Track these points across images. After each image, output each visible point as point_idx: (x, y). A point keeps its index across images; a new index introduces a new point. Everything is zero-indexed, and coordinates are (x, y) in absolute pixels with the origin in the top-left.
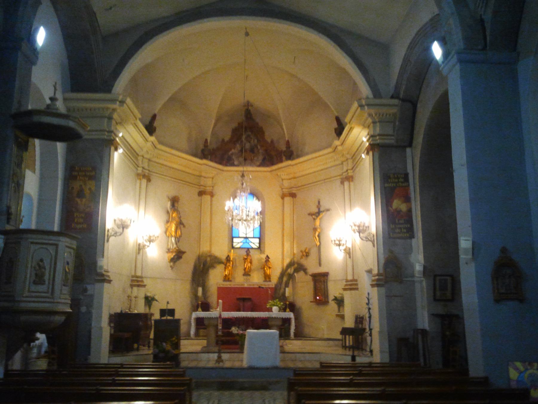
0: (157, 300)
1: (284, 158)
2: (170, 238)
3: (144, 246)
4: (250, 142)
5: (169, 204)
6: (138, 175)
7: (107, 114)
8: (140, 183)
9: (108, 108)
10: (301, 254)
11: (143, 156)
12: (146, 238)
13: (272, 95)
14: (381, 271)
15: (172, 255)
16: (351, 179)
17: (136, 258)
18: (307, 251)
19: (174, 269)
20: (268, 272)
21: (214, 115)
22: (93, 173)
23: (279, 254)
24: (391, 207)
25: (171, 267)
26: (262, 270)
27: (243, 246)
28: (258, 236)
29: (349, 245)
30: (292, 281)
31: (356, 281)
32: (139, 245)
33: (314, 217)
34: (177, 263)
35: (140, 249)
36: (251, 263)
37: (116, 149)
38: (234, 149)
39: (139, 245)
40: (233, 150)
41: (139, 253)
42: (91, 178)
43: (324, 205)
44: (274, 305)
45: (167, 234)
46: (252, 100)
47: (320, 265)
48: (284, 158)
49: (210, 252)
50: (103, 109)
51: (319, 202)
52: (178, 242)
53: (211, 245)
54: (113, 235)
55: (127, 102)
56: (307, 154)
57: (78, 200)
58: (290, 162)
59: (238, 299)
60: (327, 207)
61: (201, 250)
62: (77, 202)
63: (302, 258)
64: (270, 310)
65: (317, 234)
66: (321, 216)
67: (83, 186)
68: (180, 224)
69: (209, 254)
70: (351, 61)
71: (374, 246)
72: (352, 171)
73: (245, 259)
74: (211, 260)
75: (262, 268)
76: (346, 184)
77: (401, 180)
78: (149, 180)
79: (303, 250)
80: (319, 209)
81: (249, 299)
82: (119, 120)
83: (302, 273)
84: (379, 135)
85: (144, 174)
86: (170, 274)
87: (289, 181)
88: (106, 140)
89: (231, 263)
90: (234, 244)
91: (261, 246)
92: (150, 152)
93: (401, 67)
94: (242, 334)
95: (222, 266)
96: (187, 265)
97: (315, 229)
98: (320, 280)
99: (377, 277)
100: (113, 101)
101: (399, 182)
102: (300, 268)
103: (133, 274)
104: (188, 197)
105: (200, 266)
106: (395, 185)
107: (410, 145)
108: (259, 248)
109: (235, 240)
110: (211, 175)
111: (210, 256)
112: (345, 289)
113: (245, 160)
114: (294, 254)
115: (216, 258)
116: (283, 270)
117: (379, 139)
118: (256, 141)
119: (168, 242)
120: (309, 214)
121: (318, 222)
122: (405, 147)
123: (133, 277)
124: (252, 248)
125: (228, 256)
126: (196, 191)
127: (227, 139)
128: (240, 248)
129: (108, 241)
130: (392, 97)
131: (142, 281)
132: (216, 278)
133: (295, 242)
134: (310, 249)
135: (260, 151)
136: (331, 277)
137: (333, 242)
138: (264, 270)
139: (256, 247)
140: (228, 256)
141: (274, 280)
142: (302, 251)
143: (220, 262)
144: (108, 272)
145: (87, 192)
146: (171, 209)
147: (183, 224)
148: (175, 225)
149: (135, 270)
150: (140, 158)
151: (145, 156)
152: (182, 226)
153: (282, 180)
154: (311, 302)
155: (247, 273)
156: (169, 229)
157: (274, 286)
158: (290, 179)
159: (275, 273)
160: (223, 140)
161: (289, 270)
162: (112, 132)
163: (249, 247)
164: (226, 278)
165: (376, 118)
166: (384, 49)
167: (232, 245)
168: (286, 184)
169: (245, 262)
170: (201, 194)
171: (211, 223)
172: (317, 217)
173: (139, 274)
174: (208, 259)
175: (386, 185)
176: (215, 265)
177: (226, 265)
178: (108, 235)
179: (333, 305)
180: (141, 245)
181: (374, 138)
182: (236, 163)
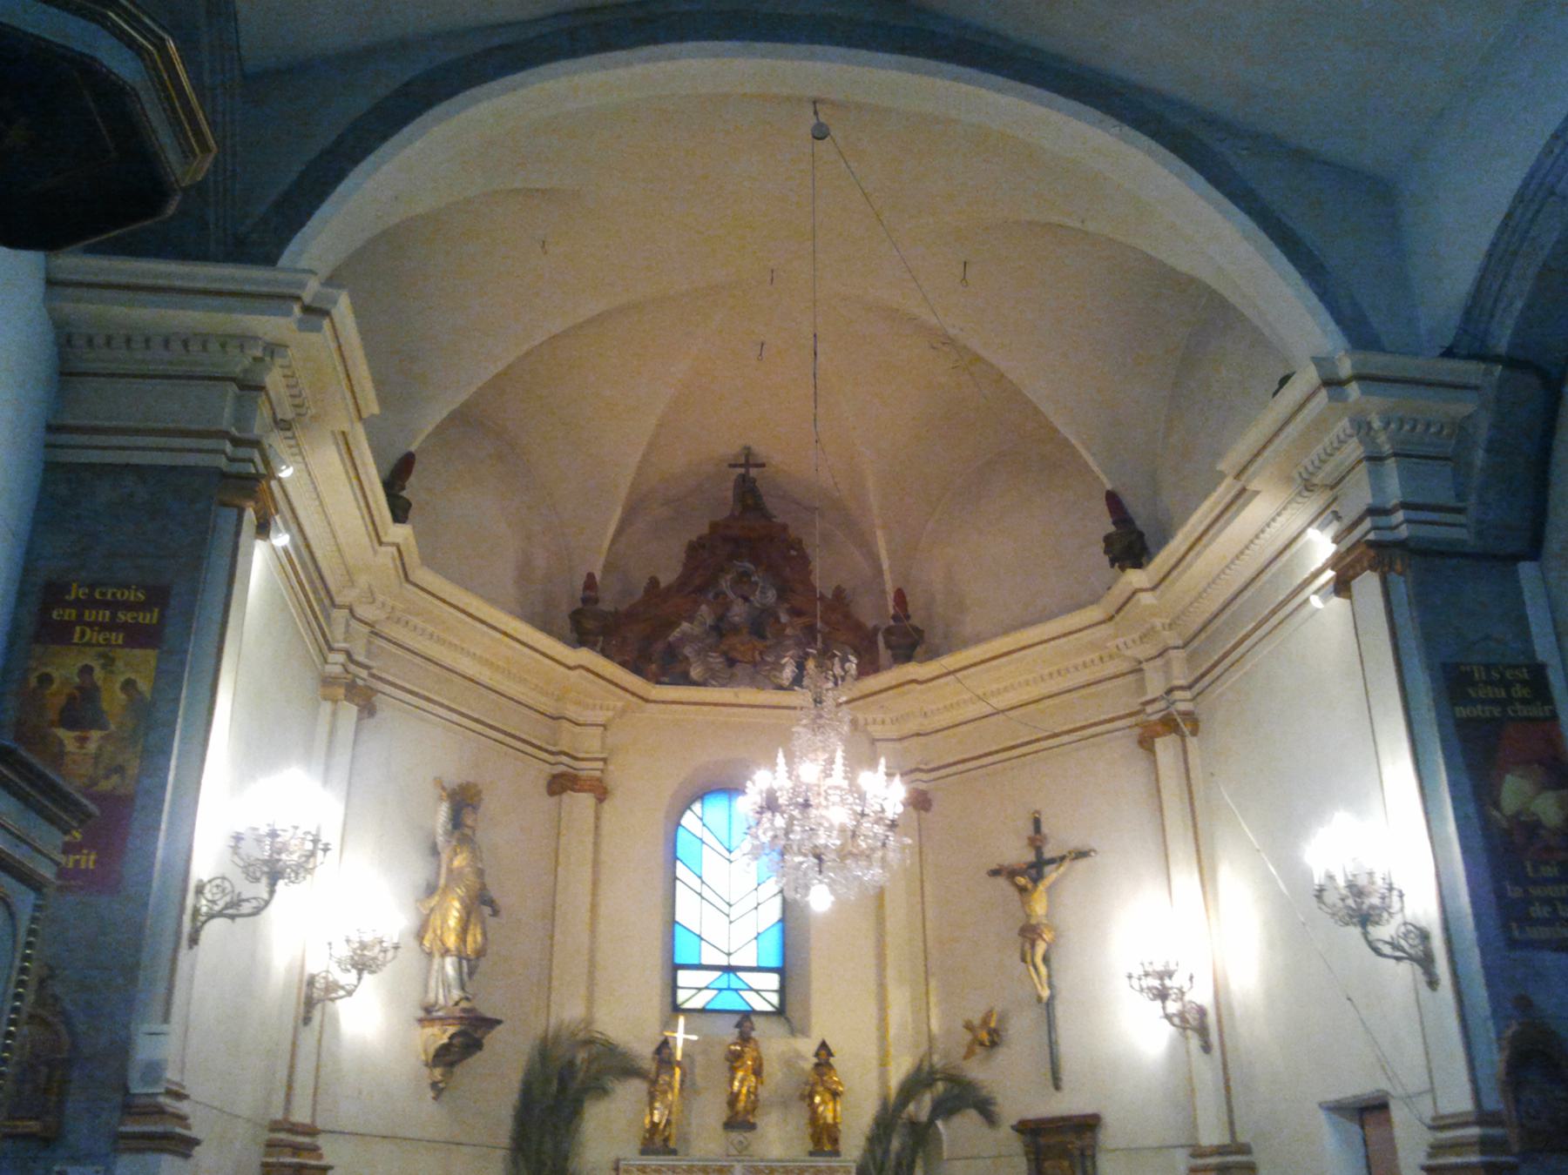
1: (884, 653)
2: (437, 960)
3: (332, 988)
4: (746, 599)
5: (443, 812)
6: (327, 682)
7: (239, 363)
8: (334, 714)
9: (244, 340)
10: (968, 1036)
11: (351, 611)
12: (344, 952)
13: (841, 430)
14: (1494, 1101)
15: (440, 1035)
17: (294, 1044)
18: (993, 1025)
19: (446, 1096)
20: (827, 1112)
21: (623, 493)
22: (149, 618)
24: (1497, 805)
25: (434, 1085)
26: (805, 1105)
28: (774, 960)
29: (1201, 995)
31: (1244, 1149)
32: (311, 982)
33: (1021, 880)
34: (458, 1069)
35: (313, 1000)
36: (757, 1072)
37: (263, 529)
38: (691, 619)
39: (311, 982)
40: (685, 625)
41: (307, 1020)
42: (140, 637)
45: (427, 943)
46: (761, 450)
47: (1057, 1083)
48: (884, 653)
49: (589, 1022)
50: (224, 341)
51: (1037, 823)
52: (471, 974)
53: (590, 1001)
54: (220, 914)
55: (334, 312)
56: (978, 640)
57: (67, 736)
58: (912, 670)
60: (1075, 841)
61: (553, 1021)
62: (61, 743)
63: (969, 1053)
65: (1041, 948)
66: (1052, 874)
67: (98, 674)
68: (481, 903)
69: (582, 1036)
70: (1251, 225)
71: (1433, 983)
72: (1188, 694)
77: (1519, 691)
79: (977, 1021)
80: (1039, 851)
82: (287, 412)
84: (1404, 506)
85: (349, 680)
86: (427, 1115)
88: (224, 475)
89: (678, 1071)
90: (682, 996)
91: (790, 998)
92: (380, 598)
93: (1505, 224)
95: (637, 1087)
99: (1474, 1131)
100: (278, 300)
101: (1510, 700)
102: (961, 1096)
103: (279, 1116)
104: (513, 792)
106: (1497, 712)
107: (1534, 549)
108: (780, 1012)
109: (684, 977)
110: (601, 716)
111: (589, 1042)
113: (731, 662)
114: (931, 1039)
115: (610, 1049)
117: (1408, 521)
118: (771, 595)
120: (995, 873)
121: (1039, 906)
122: (1516, 558)
123: (275, 1126)
124: (754, 1012)
126: (538, 772)
127: (666, 578)
128: (703, 1011)
129: (194, 940)
130: (1449, 353)
131: (314, 1150)
133: (933, 983)
134: (1003, 1018)
135: (788, 631)
136: (1109, 1137)
138: (813, 1107)
139: (770, 1008)
142: (969, 1026)
143: (627, 1068)
144: (180, 1096)
145: (113, 700)
146: (449, 834)
147: (490, 903)
150: (340, 615)
151: (360, 611)
152: (487, 910)
155: (739, 1121)
156: (436, 921)
158: (901, 739)
160: (654, 582)
161: (911, 1107)
162: (256, 443)
163: (744, 1007)
165: (1382, 438)
166: (1378, 196)
169: (733, 1070)
170: (560, 784)
171: (594, 907)
173: (301, 1116)
174: (581, 1056)
175: (1463, 712)
177: (654, 1082)
178: (196, 911)
180: (320, 984)
181: (1382, 521)
182: (695, 672)
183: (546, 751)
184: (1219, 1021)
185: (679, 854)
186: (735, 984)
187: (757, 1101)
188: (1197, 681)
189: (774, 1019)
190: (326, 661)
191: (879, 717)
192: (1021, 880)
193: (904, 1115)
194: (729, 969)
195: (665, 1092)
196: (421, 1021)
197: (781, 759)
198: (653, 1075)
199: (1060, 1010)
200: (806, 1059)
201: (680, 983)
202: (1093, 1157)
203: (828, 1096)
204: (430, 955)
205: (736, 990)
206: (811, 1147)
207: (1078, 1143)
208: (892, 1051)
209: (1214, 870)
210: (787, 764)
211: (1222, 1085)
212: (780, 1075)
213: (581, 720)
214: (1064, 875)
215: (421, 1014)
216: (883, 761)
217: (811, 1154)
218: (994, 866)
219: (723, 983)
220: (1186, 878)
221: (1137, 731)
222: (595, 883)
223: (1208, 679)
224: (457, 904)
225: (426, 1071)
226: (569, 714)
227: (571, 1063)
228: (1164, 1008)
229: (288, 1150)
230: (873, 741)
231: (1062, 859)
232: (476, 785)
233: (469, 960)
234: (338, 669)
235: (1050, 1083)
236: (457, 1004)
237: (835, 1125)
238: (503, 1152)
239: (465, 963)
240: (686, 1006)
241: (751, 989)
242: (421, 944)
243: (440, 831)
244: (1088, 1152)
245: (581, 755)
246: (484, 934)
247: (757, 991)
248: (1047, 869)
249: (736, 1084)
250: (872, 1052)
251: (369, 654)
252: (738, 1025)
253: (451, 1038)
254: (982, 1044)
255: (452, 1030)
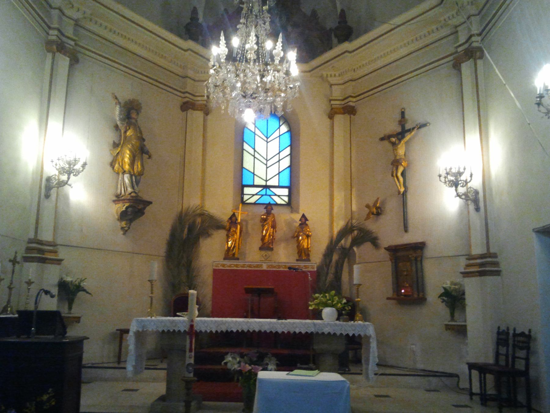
0: (84, 290)
1: (335, 40)
2: (121, 175)
8: (53, 58)
15: (121, 207)
16: (478, 54)
23: (324, 214)
25: (122, 228)
27: (262, 201)
28: (287, 183)
29: (476, 183)
30: (349, 259)
31: (495, 256)
33: (393, 140)
36: (274, 227)
39: (49, 179)
43: (414, 116)
44: (326, 305)
47: (406, 230)
51: (403, 114)
58: (346, 46)
59: (248, 291)
63: (368, 218)
64: (317, 315)
65: (401, 169)
66: (408, 137)
68: (141, 151)
69: (198, 212)
72: (479, 38)
73: (264, 221)
74: (203, 222)
75: (293, 237)
76: (466, 68)
78: (74, 60)
79: (371, 204)
80: (403, 127)
81: (270, 292)
83: (367, 246)
86: (120, 240)
87: (343, 87)
89: (239, 227)
90: (246, 197)
91: (293, 199)
94: (250, 371)
95: (222, 233)
96: (158, 228)
97: (396, 163)
98: (408, 259)
103: (32, 235)
105: (182, 231)
108: (289, 204)
109: (247, 190)
111: (202, 215)
112: (466, 274)
115: (211, 218)
116: (331, 241)
119: (117, 182)
120: (382, 139)
121: (401, 151)
123: (30, 241)
124: (277, 204)
125: (234, 215)
126: (178, 101)
128: (255, 204)
132: (211, 254)
133: (354, 190)
134: (383, 203)
136: (429, 252)
137: (443, 179)
138: (298, 242)
139: (284, 203)
140: (234, 215)
141: (316, 258)
142: (368, 206)
143: (217, 225)
146: (122, 120)
147: (147, 153)
148: (130, 151)
149: (37, 228)
151: (68, 12)
153: (331, 85)
154: (388, 299)
155: (267, 246)
157: (315, 269)
159: (318, 243)
161: (343, 242)
164: (229, 255)
167: (242, 198)
168: (337, 92)
169: (263, 226)
172: (400, 140)
173: (46, 236)
174: (199, 220)
176: (211, 231)
177: (229, 231)
179: (435, 308)
183: (180, 92)
184: (485, 196)
185: (245, 140)
186: (269, 192)
187: (273, 239)
188: (483, 30)
189: (286, 207)
190: (48, 34)
191: (333, 73)
192: (393, 140)
193: (340, 245)
194: (266, 187)
195: (233, 235)
196: (114, 201)
197: (222, 38)
198: (228, 227)
199: (409, 196)
200: (296, 222)
201: (245, 193)
202: (421, 261)
203: (305, 237)
204: (118, 173)
205: (270, 196)
206: (297, 257)
207: (415, 255)
208: (335, 219)
209: (487, 125)
210: (225, 39)
211: (484, 228)
212: (285, 229)
213: (197, 79)
214: (414, 137)
215: (115, 198)
216: (281, 35)
217: (297, 260)
218: (382, 136)
219: (263, 192)
220: (473, 136)
221: (452, 63)
222: (204, 150)
223: (490, 25)
224: (128, 152)
225: (118, 223)
226: (189, 75)
227: (194, 222)
228: (456, 190)
229: (36, 251)
230: (331, 85)
231: (413, 129)
232: (138, 101)
233: (136, 177)
234: (54, 38)
235: (402, 227)
236: (130, 194)
237: (308, 248)
238: (161, 258)
239: (134, 178)
240: (248, 202)
241: (276, 195)
242: (113, 168)
243: (117, 119)
244: (419, 259)
245: (197, 94)
246: (142, 165)
247: (279, 196)
248: (406, 134)
249: (264, 232)
250: (327, 220)
251: (74, 34)
252: (266, 208)
253: (127, 208)
254: (373, 214)
255: (127, 205)
